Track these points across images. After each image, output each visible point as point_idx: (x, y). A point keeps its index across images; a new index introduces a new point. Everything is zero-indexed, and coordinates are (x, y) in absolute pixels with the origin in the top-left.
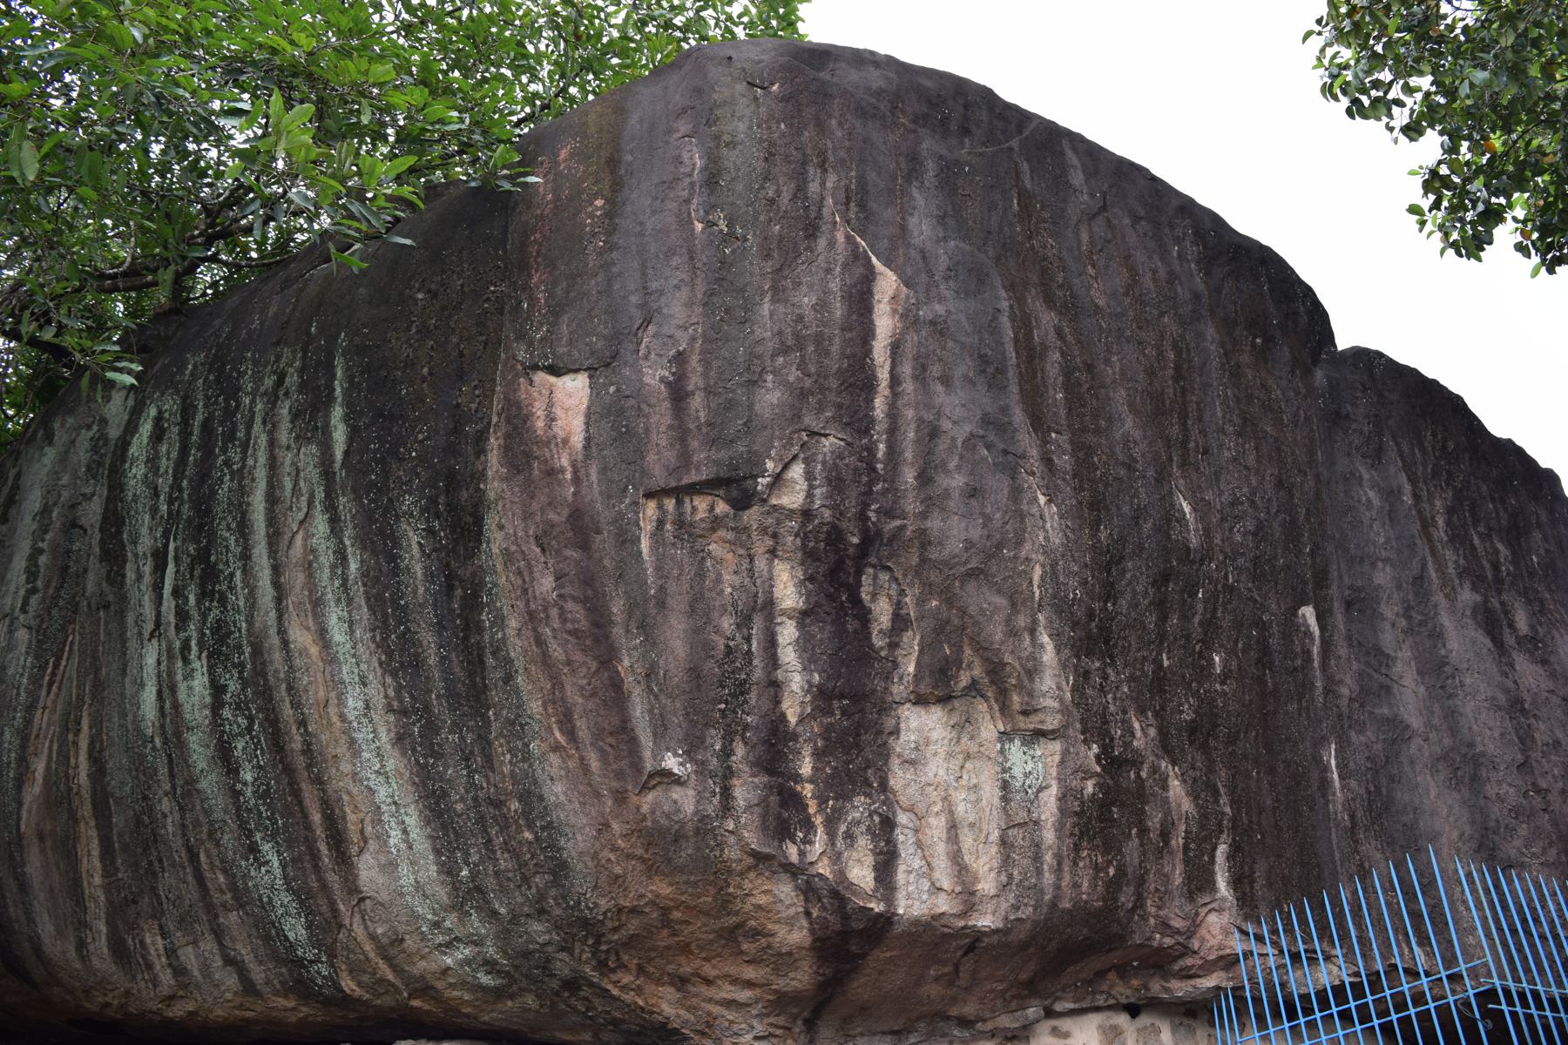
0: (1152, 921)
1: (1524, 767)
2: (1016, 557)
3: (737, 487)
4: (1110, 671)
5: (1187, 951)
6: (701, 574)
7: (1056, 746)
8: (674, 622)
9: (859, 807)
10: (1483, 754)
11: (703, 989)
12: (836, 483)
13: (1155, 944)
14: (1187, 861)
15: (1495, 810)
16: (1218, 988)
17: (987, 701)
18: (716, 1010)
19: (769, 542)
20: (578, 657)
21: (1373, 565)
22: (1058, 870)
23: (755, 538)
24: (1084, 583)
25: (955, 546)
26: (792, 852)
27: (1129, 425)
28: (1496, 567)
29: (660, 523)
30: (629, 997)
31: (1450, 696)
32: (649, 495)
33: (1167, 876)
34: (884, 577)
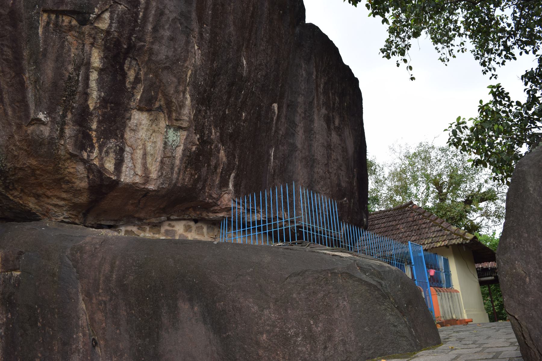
0: (207, 194)
1: (327, 165)
2: (183, 66)
3: (82, 16)
4: (208, 111)
5: (216, 204)
6: (62, 47)
7: (185, 133)
8: (49, 63)
9: (112, 143)
10: (316, 159)
11: (46, 200)
12: (121, 23)
13: (206, 201)
14: (221, 177)
15: (316, 176)
16: (224, 217)
17: (164, 113)
18: (50, 207)
19: (92, 40)
20: (7, 70)
21: (299, 95)
22: (179, 173)
23: (86, 37)
24: (205, 80)
25: (162, 57)
26: (85, 155)
27: (232, 29)
28: (334, 104)
29: (48, 23)
30: (17, 200)
31: (311, 140)
32: (45, 11)
33: (214, 180)
34: (134, 62)
